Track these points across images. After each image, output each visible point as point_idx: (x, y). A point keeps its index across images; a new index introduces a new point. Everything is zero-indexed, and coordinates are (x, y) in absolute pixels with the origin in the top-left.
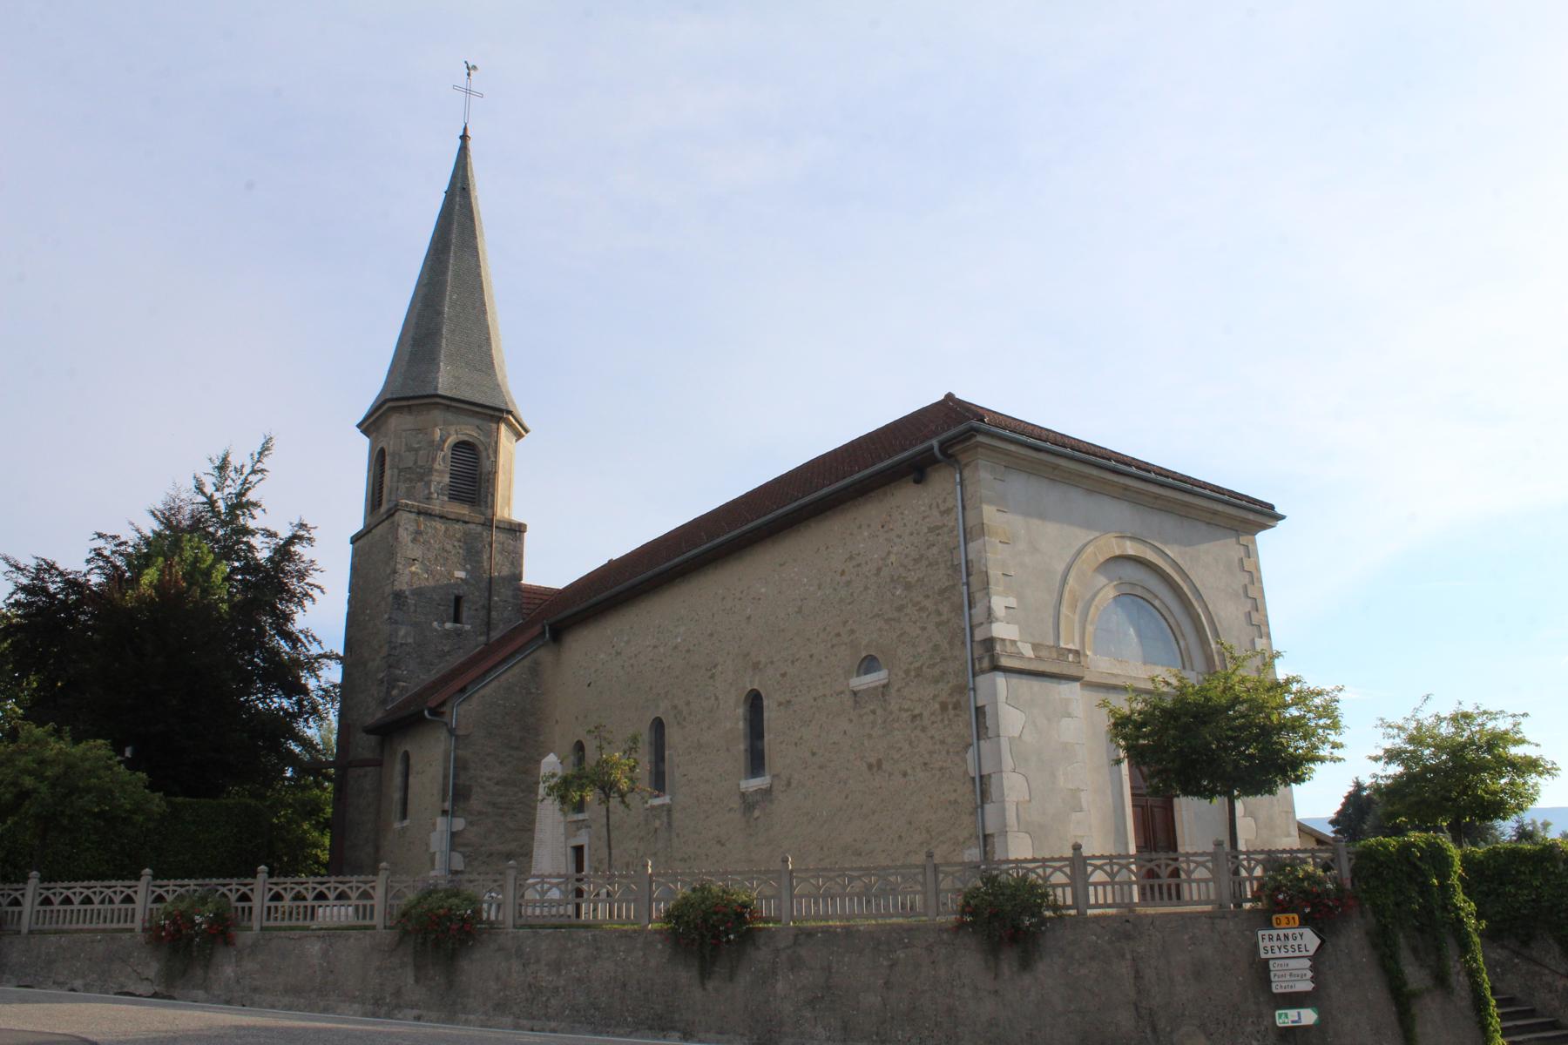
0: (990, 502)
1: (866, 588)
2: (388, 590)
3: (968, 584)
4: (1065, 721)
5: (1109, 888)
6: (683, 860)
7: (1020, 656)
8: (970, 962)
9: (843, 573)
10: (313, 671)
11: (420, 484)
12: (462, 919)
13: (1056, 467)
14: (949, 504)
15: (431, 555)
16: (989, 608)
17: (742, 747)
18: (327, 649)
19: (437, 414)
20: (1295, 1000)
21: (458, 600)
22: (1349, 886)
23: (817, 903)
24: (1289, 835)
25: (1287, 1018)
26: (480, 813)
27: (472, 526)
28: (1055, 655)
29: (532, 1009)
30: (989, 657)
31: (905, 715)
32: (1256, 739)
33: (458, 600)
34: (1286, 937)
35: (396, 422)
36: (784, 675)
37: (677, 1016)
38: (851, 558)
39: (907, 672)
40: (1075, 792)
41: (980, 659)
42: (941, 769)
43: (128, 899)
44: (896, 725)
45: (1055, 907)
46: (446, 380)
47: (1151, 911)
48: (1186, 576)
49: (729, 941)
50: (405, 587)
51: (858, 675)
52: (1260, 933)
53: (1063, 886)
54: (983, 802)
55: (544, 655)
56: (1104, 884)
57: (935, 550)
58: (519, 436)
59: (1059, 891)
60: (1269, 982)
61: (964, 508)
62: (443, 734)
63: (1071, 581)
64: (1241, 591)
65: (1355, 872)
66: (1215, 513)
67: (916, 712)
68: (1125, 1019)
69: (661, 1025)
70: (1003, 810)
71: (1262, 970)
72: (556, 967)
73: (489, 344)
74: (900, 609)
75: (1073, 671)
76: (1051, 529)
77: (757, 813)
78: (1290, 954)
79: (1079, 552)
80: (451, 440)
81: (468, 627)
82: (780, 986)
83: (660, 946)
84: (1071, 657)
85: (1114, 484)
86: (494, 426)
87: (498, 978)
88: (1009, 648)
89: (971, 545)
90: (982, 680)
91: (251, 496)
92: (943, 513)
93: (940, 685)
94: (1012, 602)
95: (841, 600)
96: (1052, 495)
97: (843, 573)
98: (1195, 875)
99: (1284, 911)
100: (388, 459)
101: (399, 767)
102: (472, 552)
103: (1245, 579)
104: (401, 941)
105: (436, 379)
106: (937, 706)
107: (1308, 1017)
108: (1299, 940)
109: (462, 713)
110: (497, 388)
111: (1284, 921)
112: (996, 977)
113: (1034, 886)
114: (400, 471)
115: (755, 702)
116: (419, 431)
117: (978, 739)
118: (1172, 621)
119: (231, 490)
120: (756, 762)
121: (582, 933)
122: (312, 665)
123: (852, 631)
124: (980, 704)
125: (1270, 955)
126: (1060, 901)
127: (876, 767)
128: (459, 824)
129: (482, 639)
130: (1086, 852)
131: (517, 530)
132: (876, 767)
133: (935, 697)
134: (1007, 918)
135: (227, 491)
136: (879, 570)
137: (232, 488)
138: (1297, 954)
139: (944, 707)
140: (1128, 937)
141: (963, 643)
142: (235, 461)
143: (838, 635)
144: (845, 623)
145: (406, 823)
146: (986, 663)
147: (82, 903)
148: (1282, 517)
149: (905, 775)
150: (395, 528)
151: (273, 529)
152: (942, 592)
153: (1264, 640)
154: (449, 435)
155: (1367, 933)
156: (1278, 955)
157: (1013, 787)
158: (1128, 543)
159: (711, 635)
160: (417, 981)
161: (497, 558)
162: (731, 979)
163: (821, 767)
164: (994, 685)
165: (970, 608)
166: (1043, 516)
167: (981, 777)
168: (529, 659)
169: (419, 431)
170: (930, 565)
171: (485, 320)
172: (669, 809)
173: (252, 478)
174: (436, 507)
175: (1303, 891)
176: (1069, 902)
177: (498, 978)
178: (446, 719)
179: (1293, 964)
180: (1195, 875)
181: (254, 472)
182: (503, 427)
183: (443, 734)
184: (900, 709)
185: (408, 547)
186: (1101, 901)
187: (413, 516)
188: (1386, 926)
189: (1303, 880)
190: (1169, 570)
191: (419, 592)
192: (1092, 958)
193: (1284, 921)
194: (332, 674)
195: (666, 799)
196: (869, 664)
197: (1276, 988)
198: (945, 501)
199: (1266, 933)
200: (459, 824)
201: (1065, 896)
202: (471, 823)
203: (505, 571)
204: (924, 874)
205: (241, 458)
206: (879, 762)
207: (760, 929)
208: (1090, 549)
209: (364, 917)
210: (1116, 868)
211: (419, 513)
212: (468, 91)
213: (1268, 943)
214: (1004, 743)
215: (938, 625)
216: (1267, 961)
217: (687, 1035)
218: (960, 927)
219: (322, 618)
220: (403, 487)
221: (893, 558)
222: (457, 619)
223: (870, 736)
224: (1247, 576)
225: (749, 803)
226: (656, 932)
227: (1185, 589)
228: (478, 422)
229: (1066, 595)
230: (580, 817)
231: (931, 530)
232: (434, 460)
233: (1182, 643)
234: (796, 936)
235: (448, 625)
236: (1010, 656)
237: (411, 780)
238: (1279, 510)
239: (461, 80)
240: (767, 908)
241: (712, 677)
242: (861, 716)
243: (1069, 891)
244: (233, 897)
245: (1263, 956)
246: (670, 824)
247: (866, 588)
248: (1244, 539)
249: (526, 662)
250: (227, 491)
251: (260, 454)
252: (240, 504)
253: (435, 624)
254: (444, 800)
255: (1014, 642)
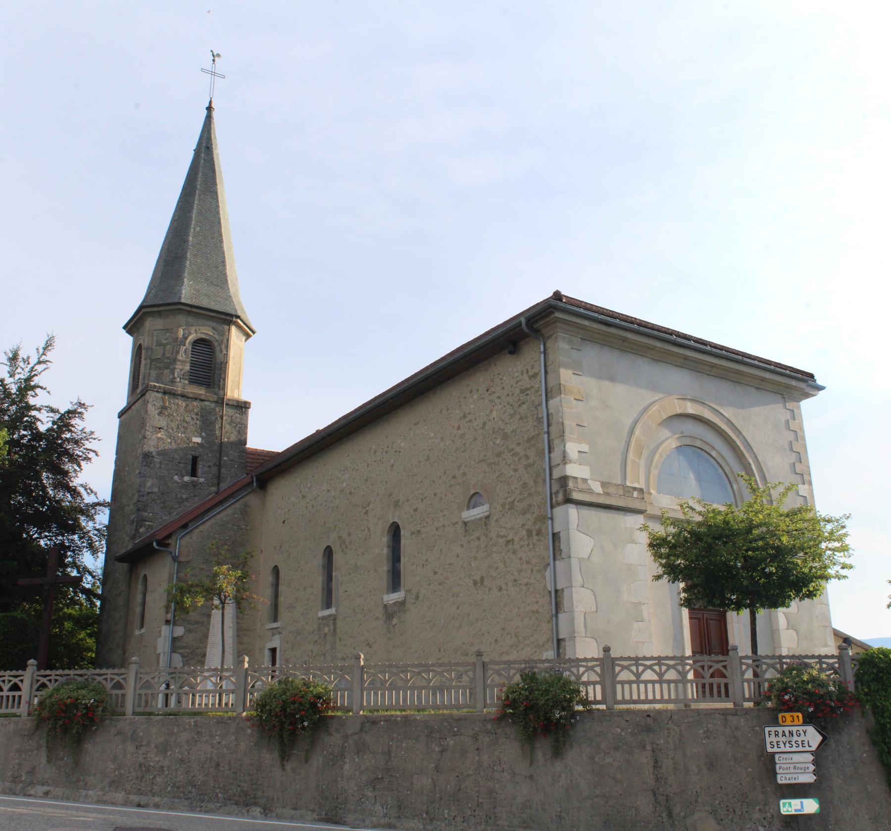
0: (567, 367)
1: (475, 439)
2: (139, 451)
3: (548, 433)
4: (629, 547)
5: (634, 686)
6: (343, 659)
7: (591, 492)
8: (509, 749)
9: (459, 428)
10: (91, 518)
11: (167, 371)
12: (86, 707)
13: (625, 340)
14: (536, 370)
15: (174, 425)
16: (564, 451)
17: (385, 568)
18: (101, 499)
19: (181, 318)
20: (798, 791)
21: (195, 460)
22: (851, 688)
23: (434, 694)
24: (826, 645)
25: (790, 807)
26: (197, 623)
27: (207, 403)
28: (621, 492)
29: (140, 785)
30: (563, 492)
31: (501, 541)
32: (774, 558)
33: (195, 460)
34: (791, 733)
35: (151, 324)
36: (416, 510)
37: (259, 794)
38: (465, 416)
39: (503, 506)
40: (637, 605)
41: (557, 493)
42: (527, 584)
43: (15, 688)
44: (495, 549)
45: (585, 702)
46: (187, 292)
47: (703, 706)
48: (739, 433)
49: (303, 728)
50: (152, 449)
51: (468, 509)
52: (767, 729)
53: (594, 683)
54: (557, 612)
55: (252, 500)
56: (653, 682)
57: (524, 407)
58: (248, 336)
59: (590, 689)
60: (775, 774)
61: (546, 372)
62: (168, 560)
63: (637, 432)
64: (787, 447)
65: (859, 678)
66: (763, 380)
67: (509, 538)
68: (644, 805)
69: (245, 801)
70: (572, 620)
71: (769, 763)
72: (163, 749)
73: (224, 266)
74: (498, 455)
75: (638, 505)
76: (620, 389)
77: (395, 621)
78: (794, 749)
79: (646, 409)
80: (192, 338)
81: (202, 480)
82: (347, 767)
83: (249, 731)
84: (635, 494)
85: (678, 355)
86: (226, 327)
87: (115, 759)
88: (581, 485)
89: (551, 402)
90: (558, 511)
91: (36, 381)
92: (531, 377)
93: (528, 516)
94: (585, 447)
95: (457, 449)
96: (622, 363)
97: (459, 428)
98: (644, 677)
99: (790, 710)
100: (143, 352)
101: (140, 587)
102: (207, 423)
103: (791, 437)
104: (38, 727)
105: (180, 291)
106: (525, 533)
107: (810, 806)
108: (802, 737)
109: (182, 545)
110: (229, 297)
111: (789, 719)
112: (531, 764)
113: (568, 682)
114: (152, 361)
115: (395, 531)
116: (167, 330)
117: (555, 560)
118: (726, 469)
119: (22, 377)
120: (395, 581)
121: (187, 719)
122: (88, 511)
123: (464, 474)
124: (556, 531)
125: (776, 750)
126: (591, 698)
127: (479, 583)
128: (179, 631)
129: (214, 489)
130: (613, 654)
131: (243, 407)
132: (479, 583)
133: (523, 525)
134: (543, 712)
135: (17, 377)
136: (484, 424)
137: (21, 374)
138: (801, 749)
139: (529, 533)
140: (649, 730)
141: (545, 481)
142: (22, 354)
143: (454, 477)
144: (459, 468)
145: (143, 630)
146: (560, 497)
147: (11, 689)
148: (821, 388)
149: (500, 589)
150: (146, 403)
151: (54, 406)
152: (530, 440)
153: (806, 486)
154: (190, 334)
155: (868, 732)
156: (783, 749)
157: (581, 600)
158: (689, 404)
159: (367, 480)
160: (49, 762)
161: (227, 427)
162: (306, 762)
163: (440, 584)
164: (567, 514)
165: (550, 452)
166: (612, 379)
167: (556, 591)
168: (241, 502)
169: (167, 330)
170: (521, 418)
171: (222, 247)
172: (334, 618)
173: (39, 368)
174: (179, 389)
175: (808, 693)
176: (599, 697)
177: (115, 759)
178: (171, 549)
179: (796, 758)
180: (644, 677)
181: (39, 362)
182: (233, 329)
183: (168, 560)
184: (498, 536)
185: (154, 418)
186: (658, 697)
187: (160, 395)
188: (885, 726)
189: (807, 682)
190: (724, 426)
191: (163, 453)
192: (616, 749)
193: (789, 719)
194: (103, 518)
195: (332, 611)
196: (473, 500)
197: (781, 780)
198: (532, 367)
199: (773, 729)
200: (179, 631)
201: (595, 693)
202: (189, 631)
203: (233, 438)
204: (474, 673)
205: (30, 351)
206: (482, 579)
207: (332, 717)
208: (655, 408)
209: (13, 707)
210: (664, 668)
211: (165, 393)
212: (213, 73)
213: (773, 739)
214: (575, 563)
215: (526, 467)
216: (773, 754)
217: (267, 812)
218: (502, 718)
219: (95, 477)
220: (154, 373)
221: (494, 414)
222: (194, 473)
223: (475, 558)
224: (792, 434)
225: (390, 613)
226: (248, 719)
227: (738, 442)
228: (214, 324)
229: (633, 444)
230: (275, 625)
231: (522, 391)
232: (178, 352)
233: (735, 487)
234: (363, 724)
235: (187, 479)
236: (581, 491)
237: (147, 596)
238: (819, 382)
239: (209, 65)
240: (342, 699)
241: (366, 513)
242: (469, 542)
243: (598, 688)
244: (108, 685)
245: (769, 750)
246: (335, 630)
247: (475, 439)
248: (789, 405)
249: (237, 505)
250: (17, 377)
251: (45, 349)
252: (27, 386)
253: (176, 478)
254: (167, 613)
255: (585, 480)
